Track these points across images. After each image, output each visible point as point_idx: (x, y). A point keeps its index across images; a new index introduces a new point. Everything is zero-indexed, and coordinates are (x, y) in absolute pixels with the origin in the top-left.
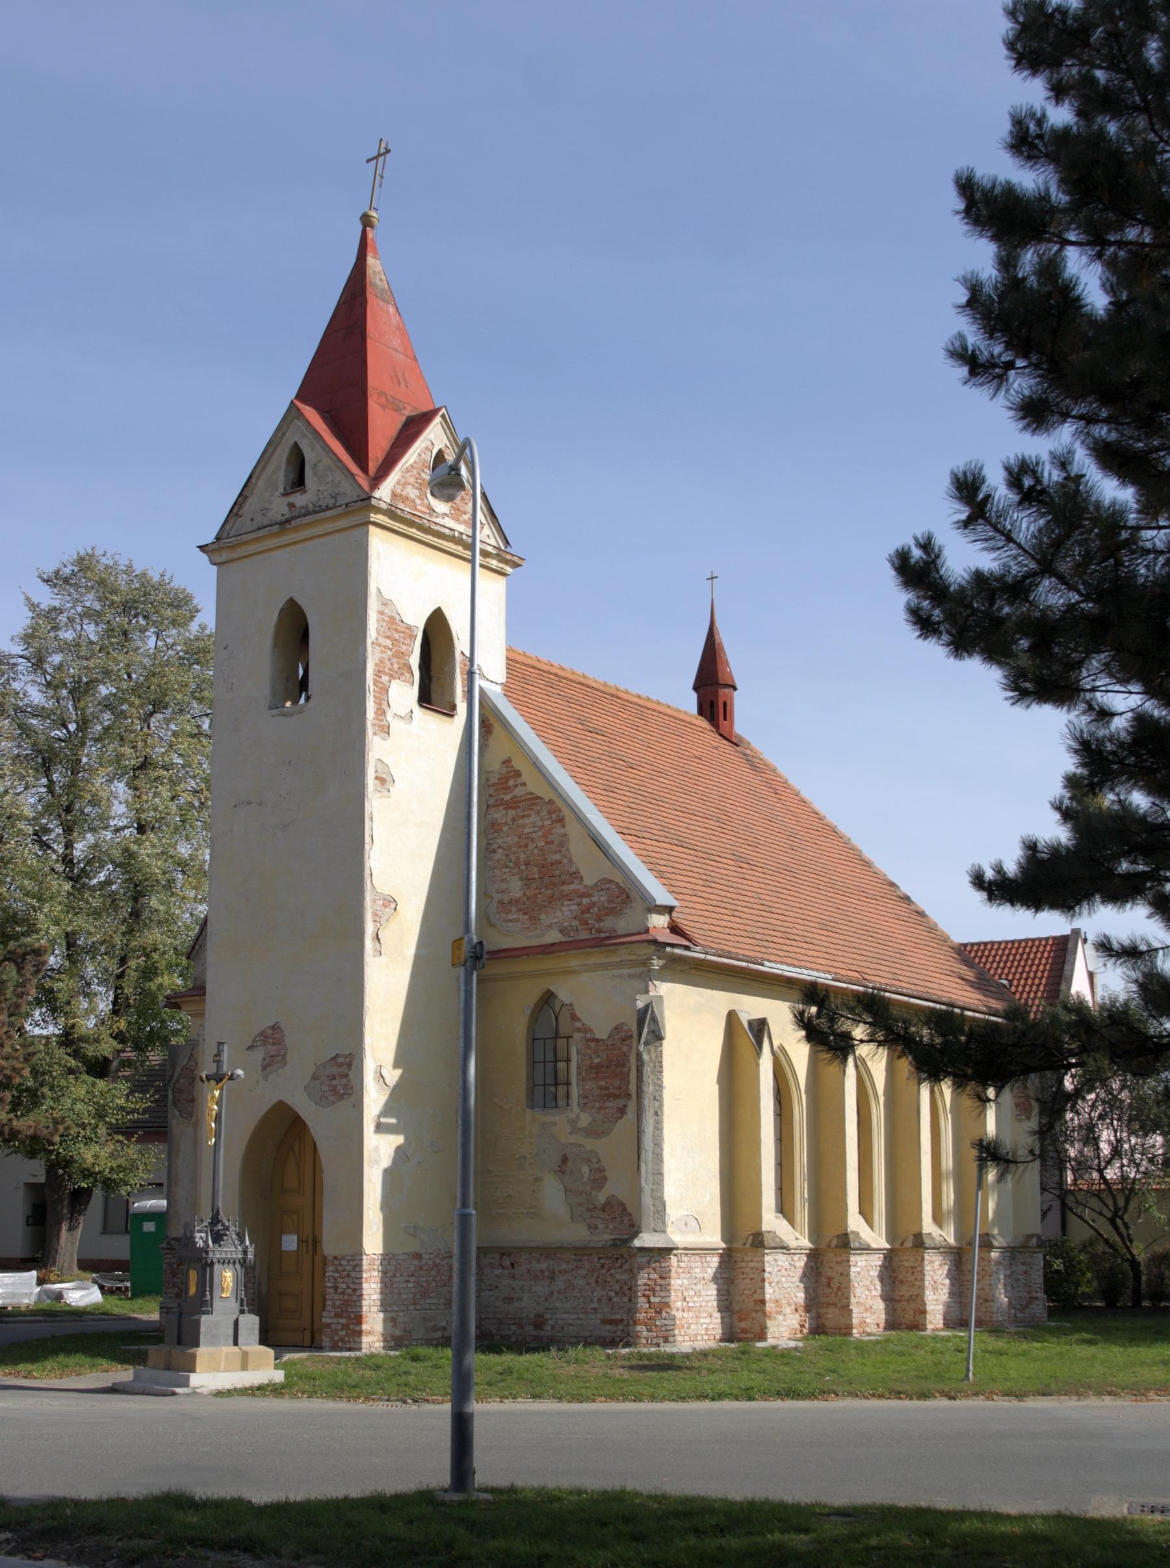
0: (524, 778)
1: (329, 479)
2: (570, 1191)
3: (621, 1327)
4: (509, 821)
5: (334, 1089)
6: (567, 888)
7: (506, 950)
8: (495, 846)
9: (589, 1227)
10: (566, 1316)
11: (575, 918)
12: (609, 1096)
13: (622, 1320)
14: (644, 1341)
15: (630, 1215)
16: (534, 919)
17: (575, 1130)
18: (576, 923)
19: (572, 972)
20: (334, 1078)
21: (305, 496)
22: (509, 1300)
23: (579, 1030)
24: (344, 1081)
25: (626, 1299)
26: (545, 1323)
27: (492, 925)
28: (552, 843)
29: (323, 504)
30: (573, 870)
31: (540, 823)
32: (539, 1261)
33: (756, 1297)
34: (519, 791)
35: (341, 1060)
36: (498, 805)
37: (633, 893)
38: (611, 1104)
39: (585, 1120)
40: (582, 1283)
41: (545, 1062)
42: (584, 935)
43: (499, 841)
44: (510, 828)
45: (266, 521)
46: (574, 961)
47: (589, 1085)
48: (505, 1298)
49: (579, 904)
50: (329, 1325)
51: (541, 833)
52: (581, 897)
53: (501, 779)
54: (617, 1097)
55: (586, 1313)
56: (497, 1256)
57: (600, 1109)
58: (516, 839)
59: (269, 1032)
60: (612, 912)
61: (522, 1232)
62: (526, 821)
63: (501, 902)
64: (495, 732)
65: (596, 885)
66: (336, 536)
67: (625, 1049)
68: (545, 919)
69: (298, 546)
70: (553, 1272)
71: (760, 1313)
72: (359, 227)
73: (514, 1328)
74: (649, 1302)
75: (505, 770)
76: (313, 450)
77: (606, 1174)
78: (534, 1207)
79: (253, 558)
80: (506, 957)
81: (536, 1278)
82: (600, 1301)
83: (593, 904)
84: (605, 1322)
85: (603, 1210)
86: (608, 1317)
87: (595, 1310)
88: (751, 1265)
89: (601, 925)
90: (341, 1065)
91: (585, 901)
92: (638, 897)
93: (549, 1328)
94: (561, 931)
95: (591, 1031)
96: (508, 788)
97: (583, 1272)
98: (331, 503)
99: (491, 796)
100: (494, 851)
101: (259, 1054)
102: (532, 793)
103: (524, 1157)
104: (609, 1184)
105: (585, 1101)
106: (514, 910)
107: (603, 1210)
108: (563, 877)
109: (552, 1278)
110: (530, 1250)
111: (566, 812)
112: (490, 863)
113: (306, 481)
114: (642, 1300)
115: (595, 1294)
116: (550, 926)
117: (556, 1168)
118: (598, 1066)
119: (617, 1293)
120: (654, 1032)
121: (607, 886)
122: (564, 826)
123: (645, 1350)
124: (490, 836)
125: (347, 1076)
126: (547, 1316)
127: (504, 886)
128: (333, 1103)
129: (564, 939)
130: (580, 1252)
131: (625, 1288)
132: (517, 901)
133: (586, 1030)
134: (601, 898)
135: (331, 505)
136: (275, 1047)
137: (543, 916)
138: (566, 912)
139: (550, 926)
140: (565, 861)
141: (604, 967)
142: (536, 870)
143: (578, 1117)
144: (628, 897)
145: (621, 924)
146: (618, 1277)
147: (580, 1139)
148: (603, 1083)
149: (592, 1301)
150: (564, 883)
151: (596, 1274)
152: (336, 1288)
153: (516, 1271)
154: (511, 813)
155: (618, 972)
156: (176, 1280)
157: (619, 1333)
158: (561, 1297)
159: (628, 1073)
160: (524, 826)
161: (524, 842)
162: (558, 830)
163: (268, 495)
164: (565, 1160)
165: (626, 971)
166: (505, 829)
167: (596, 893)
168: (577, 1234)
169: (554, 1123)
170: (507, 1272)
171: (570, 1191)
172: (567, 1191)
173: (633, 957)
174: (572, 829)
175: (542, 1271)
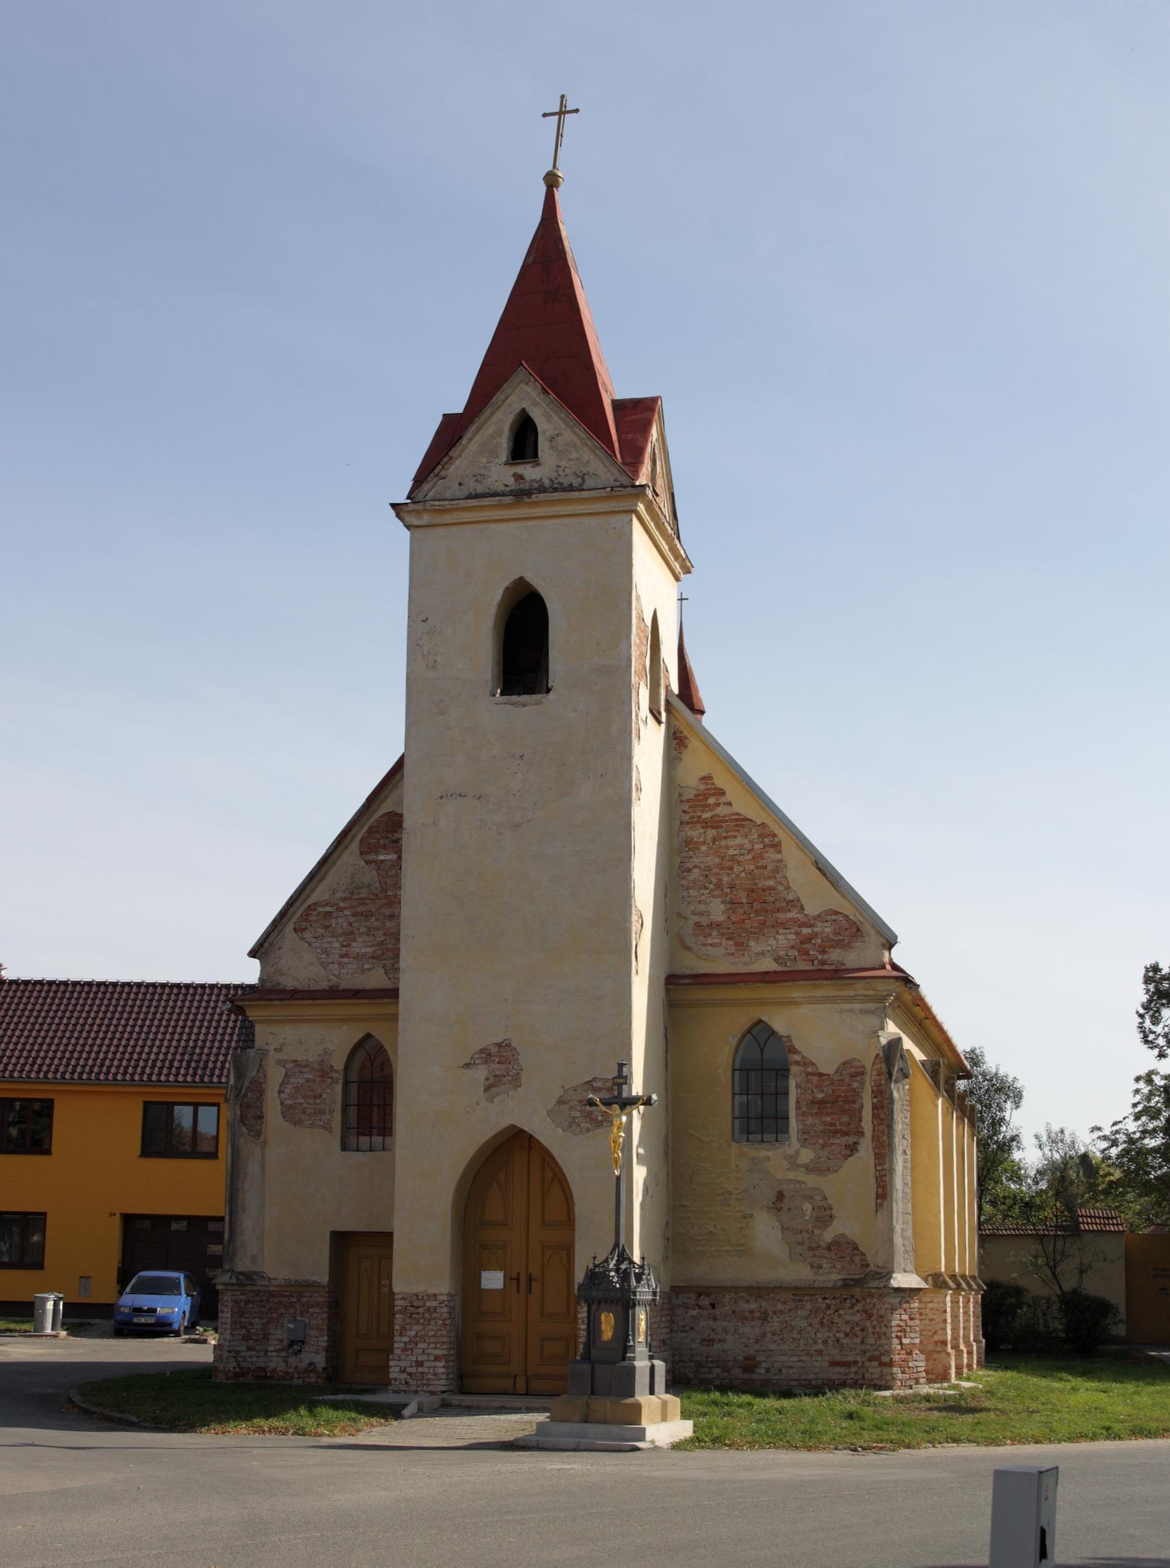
0: (729, 797)
1: (574, 456)
2: (788, 1229)
3: (854, 1369)
4: (709, 840)
6: (782, 916)
7: (704, 975)
8: (690, 865)
9: (812, 1266)
10: (785, 1358)
11: (793, 947)
12: (836, 1133)
13: (856, 1362)
14: (899, 1383)
15: (863, 1254)
16: (740, 945)
17: (793, 1164)
19: (794, 1003)
21: (537, 469)
22: (708, 1342)
23: (797, 1063)
25: (859, 1340)
26: (758, 1365)
27: (688, 948)
28: (765, 867)
29: (566, 482)
30: (790, 897)
31: (749, 846)
32: (747, 1301)
33: (936, 1338)
34: (722, 811)
35: (599, 1084)
36: (697, 822)
37: (867, 927)
38: (838, 1141)
39: (806, 1155)
40: (803, 1324)
41: (762, 1094)
42: (803, 966)
43: (696, 860)
44: (709, 848)
45: (480, 489)
47: (810, 1120)
48: (703, 1340)
49: (797, 934)
51: (750, 857)
52: (800, 926)
53: (696, 796)
55: (808, 1354)
56: (693, 1295)
58: (717, 860)
59: (494, 1050)
60: (838, 944)
61: (725, 1270)
62: (730, 842)
63: (698, 925)
64: (690, 746)
65: (819, 916)
66: (586, 520)
67: (855, 1085)
68: (755, 946)
69: (531, 523)
70: (766, 1312)
71: (943, 1354)
72: (543, 189)
73: (718, 1370)
74: (901, 1343)
75: (703, 787)
76: (548, 421)
77: (834, 1212)
78: (741, 1245)
79: (464, 527)
80: (709, 984)
81: (744, 1319)
82: (825, 1342)
83: (815, 935)
84: (834, 1364)
85: (829, 1248)
86: (838, 1358)
87: (820, 1352)
88: (930, 1305)
89: (825, 957)
91: (805, 931)
92: (873, 932)
93: (763, 1371)
94: (775, 960)
95: (813, 1064)
96: (708, 806)
97: (804, 1313)
98: (576, 482)
99: (685, 812)
100: (689, 870)
101: (481, 1073)
102: (738, 814)
103: (730, 1193)
105: (806, 1136)
106: (715, 933)
108: (778, 905)
109: (765, 1318)
110: (736, 1289)
111: (782, 836)
112: (684, 882)
113: (540, 453)
114: (896, 1341)
115: (819, 1335)
116: (762, 954)
117: (770, 1204)
118: (822, 1102)
119: (847, 1335)
120: (902, 1069)
121: (833, 917)
122: (780, 852)
123: (901, 1392)
124: (684, 854)
126: (760, 1358)
127: (703, 907)
128: (588, 1130)
130: (799, 1292)
131: (857, 1329)
133: (807, 1063)
135: (576, 484)
136: (503, 1066)
137: (752, 943)
138: (783, 940)
139: (762, 954)
140: (781, 888)
141: (833, 1000)
143: (797, 1152)
144: (858, 930)
145: (851, 958)
146: (848, 1318)
147: (801, 1176)
148: (828, 1119)
149: (815, 1343)
151: (821, 1315)
153: (718, 1312)
154: (711, 833)
156: (243, 1320)
157: (852, 1376)
158: (775, 1338)
159: (860, 1111)
160: (727, 847)
161: (729, 863)
162: (772, 855)
163: (484, 460)
164: (780, 1196)
165: (857, 1006)
166: (703, 848)
167: (819, 924)
168: (800, 1273)
169: (768, 1159)
170: (706, 1313)
171: (788, 1229)
172: (784, 1229)
173: (871, 993)
174: (791, 855)
175: (752, 1312)
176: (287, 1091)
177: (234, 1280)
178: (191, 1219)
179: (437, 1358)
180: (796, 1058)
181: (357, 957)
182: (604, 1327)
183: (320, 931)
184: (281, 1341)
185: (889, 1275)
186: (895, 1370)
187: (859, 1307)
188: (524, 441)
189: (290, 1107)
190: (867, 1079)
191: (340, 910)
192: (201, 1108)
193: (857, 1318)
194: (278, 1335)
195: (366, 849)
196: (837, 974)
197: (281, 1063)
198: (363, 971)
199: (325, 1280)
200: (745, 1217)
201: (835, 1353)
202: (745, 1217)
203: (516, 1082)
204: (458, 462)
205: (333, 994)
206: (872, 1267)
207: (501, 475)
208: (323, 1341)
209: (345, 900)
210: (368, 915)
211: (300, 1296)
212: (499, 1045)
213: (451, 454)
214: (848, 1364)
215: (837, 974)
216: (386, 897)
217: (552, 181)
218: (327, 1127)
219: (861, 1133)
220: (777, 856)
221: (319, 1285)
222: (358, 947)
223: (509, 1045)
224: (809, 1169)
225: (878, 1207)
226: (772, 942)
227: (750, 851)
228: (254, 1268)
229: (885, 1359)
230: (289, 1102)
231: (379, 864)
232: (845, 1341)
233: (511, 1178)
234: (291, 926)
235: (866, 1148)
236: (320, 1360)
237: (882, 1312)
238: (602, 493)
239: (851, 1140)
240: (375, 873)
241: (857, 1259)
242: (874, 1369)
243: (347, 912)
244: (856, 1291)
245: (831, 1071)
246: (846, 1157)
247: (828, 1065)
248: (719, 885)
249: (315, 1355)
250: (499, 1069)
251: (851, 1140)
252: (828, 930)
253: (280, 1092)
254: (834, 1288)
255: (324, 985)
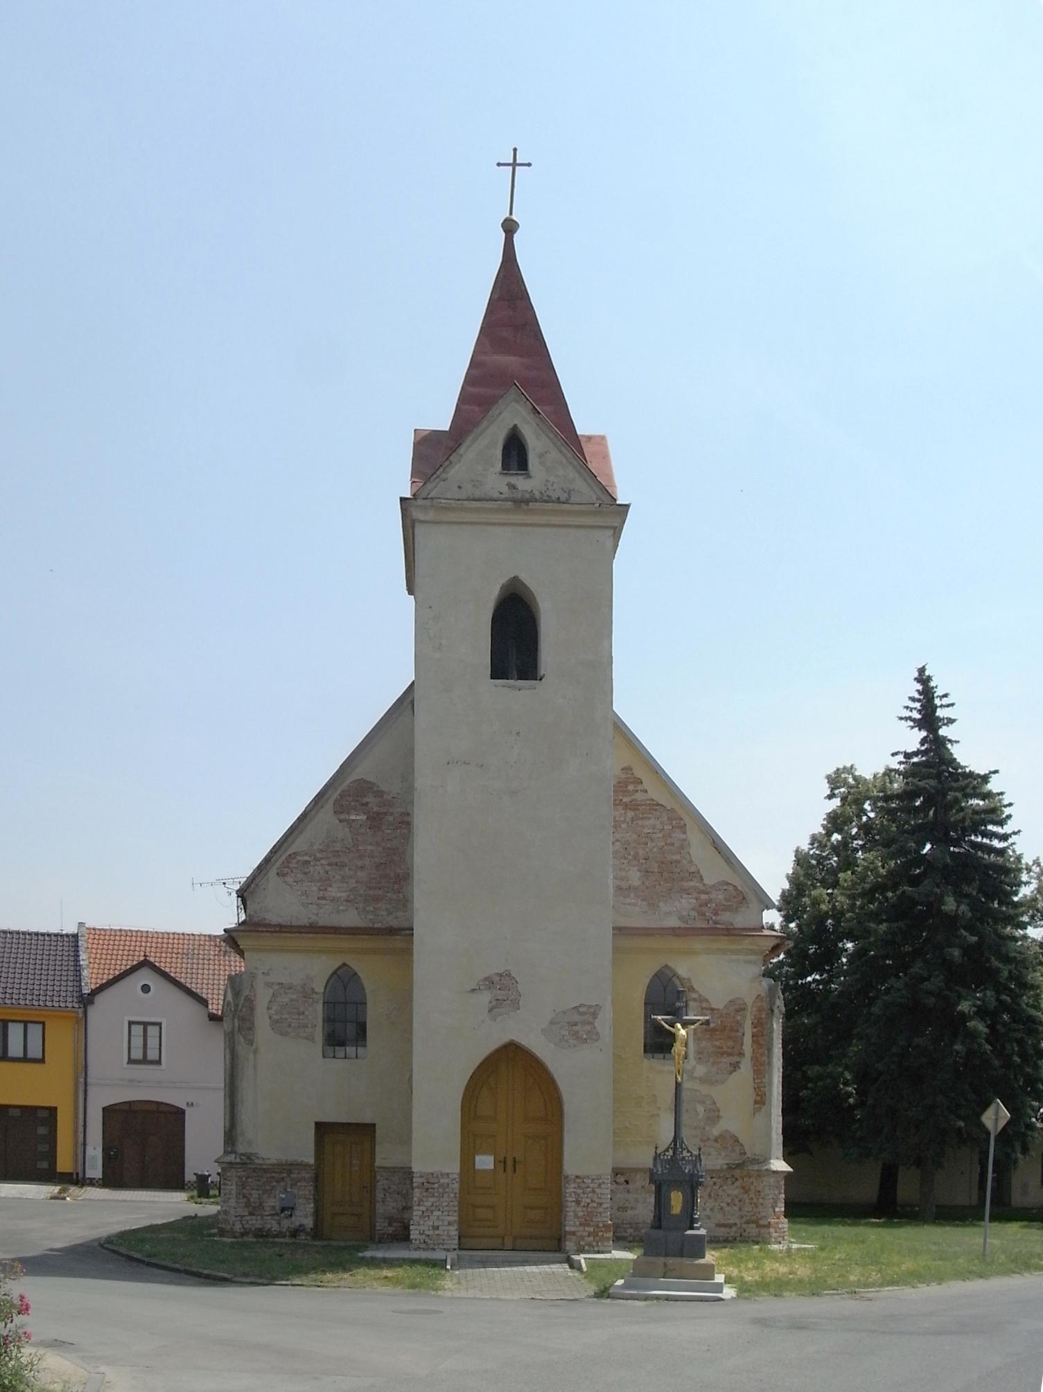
0: (646, 785)
3: (734, 1229)
4: (628, 820)
5: (576, 1035)
6: (686, 884)
18: (694, 914)
20: (576, 1024)
23: (695, 1000)
24: (588, 1028)
25: (736, 1208)
29: (554, 496)
30: (692, 870)
31: (660, 827)
34: (639, 796)
37: (750, 896)
39: (701, 1070)
42: (699, 924)
45: (477, 494)
46: (697, 944)
47: (704, 1044)
50: (574, 1233)
51: (660, 835)
54: (730, 1054)
57: (714, 1063)
58: (635, 836)
59: (496, 979)
60: (727, 909)
62: (647, 823)
68: (663, 907)
75: (624, 776)
83: (710, 901)
85: (716, 1140)
86: (723, 1222)
89: (718, 918)
90: (583, 1014)
91: (703, 897)
98: (563, 497)
101: (485, 998)
104: (722, 1121)
107: (716, 1140)
111: (687, 820)
116: (669, 913)
125: (591, 1023)
127: (623, 874)
129: (683, 925)
132: (636, 889)
134: (720, 897)
135: (563, 499)
137: (661, 904)
138: (685, 904)
141: (724, 952)
142: (656, 865)
143: (694, 1068)
145: (739, 920)
146: (730, 1192)
148: (717, 1043)
150: (682, 879)
152: (578, 1202)
153: (630, 1187)
154: (630, 814)
155: (735, 957)
160: (643, 827)
162: (678, 835)
165: (742, 957)
174: (694, 837)
176: (274, 1008)
177: (238, 1160)
178: (23, 1108)
179: (450, 1224)
180: (694, 996)
181: (333, 900)
182: (673, 1203)
183: (300, 876)
184: (274, 1207)
185: (766, 1160)
186: (772, 1230)
187: (738, 1184)
188: (515, 454)
189: (277, 1021)
190: (748, 1014)
191: (316, 859)
192: (30, 1026)
193: (736, 1192)
194: (271, 1202)
195: (340, 809)
196: (730, 932)
197: (269, 985)
198: (338, 912)
199: (312, 1161)
200: (653, 1116)
201: (719, 1217)
202: (653, 1116)
203: (515, 1005)
204: (457, 467)
205: (314, 929)
206: (749, 1155)
207: (495, 481)
208: (310, 1207)
209: (321, 851)
210: (343, 865)
211: (290, 1172)
212: (501, 975)
213: (451, 458)
214: (730, 1226)
215: (730, 932)
216: (358, 851)
217: (510, 227)
218: (311, 1038)
219: (741, 1054)
220: (682, 836)
221: (307, 1165)
222: (333, 892)
223: (509, 975)
224: (703, 1080)
225: (756, 1111)
226: (677, 904)
227: (661, 830)
228: (250, 1150)
229: (763, 1222)
230: (276, 1017)
231: (350, 823)
232: (727, 1209)
233: (513, 1084)
234: (273, 871)
235: (746, 1066)
236: (309, 1223)
237: (760, 1188)
238: (591, 508)
239: (735, 1059)
240: (347, 830)
241: (737, 1149)
242: (752, 1230)
243: (323, 862)
244: (737, 1173)
245: (720, 1006)
246: (731, 1073)
247: (718, 1002)
248: (636, 857)
249: (304, 1217)
250: (501, 995)
251: (735, 1059)
252: (720, 897)
253: (268, 1008)
254: (721, 1170)
255: (304, 921)
